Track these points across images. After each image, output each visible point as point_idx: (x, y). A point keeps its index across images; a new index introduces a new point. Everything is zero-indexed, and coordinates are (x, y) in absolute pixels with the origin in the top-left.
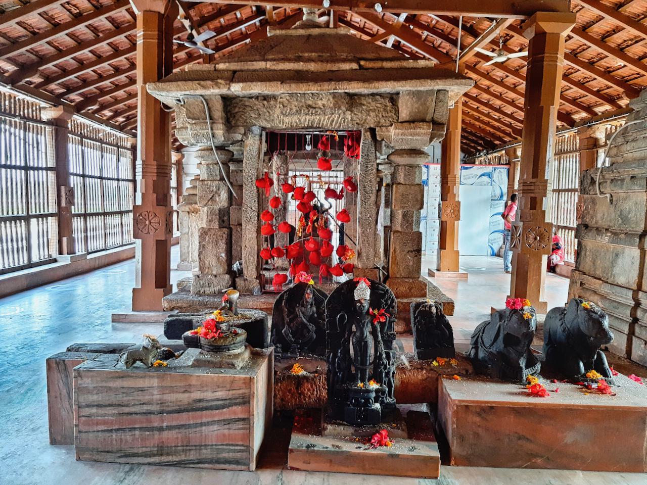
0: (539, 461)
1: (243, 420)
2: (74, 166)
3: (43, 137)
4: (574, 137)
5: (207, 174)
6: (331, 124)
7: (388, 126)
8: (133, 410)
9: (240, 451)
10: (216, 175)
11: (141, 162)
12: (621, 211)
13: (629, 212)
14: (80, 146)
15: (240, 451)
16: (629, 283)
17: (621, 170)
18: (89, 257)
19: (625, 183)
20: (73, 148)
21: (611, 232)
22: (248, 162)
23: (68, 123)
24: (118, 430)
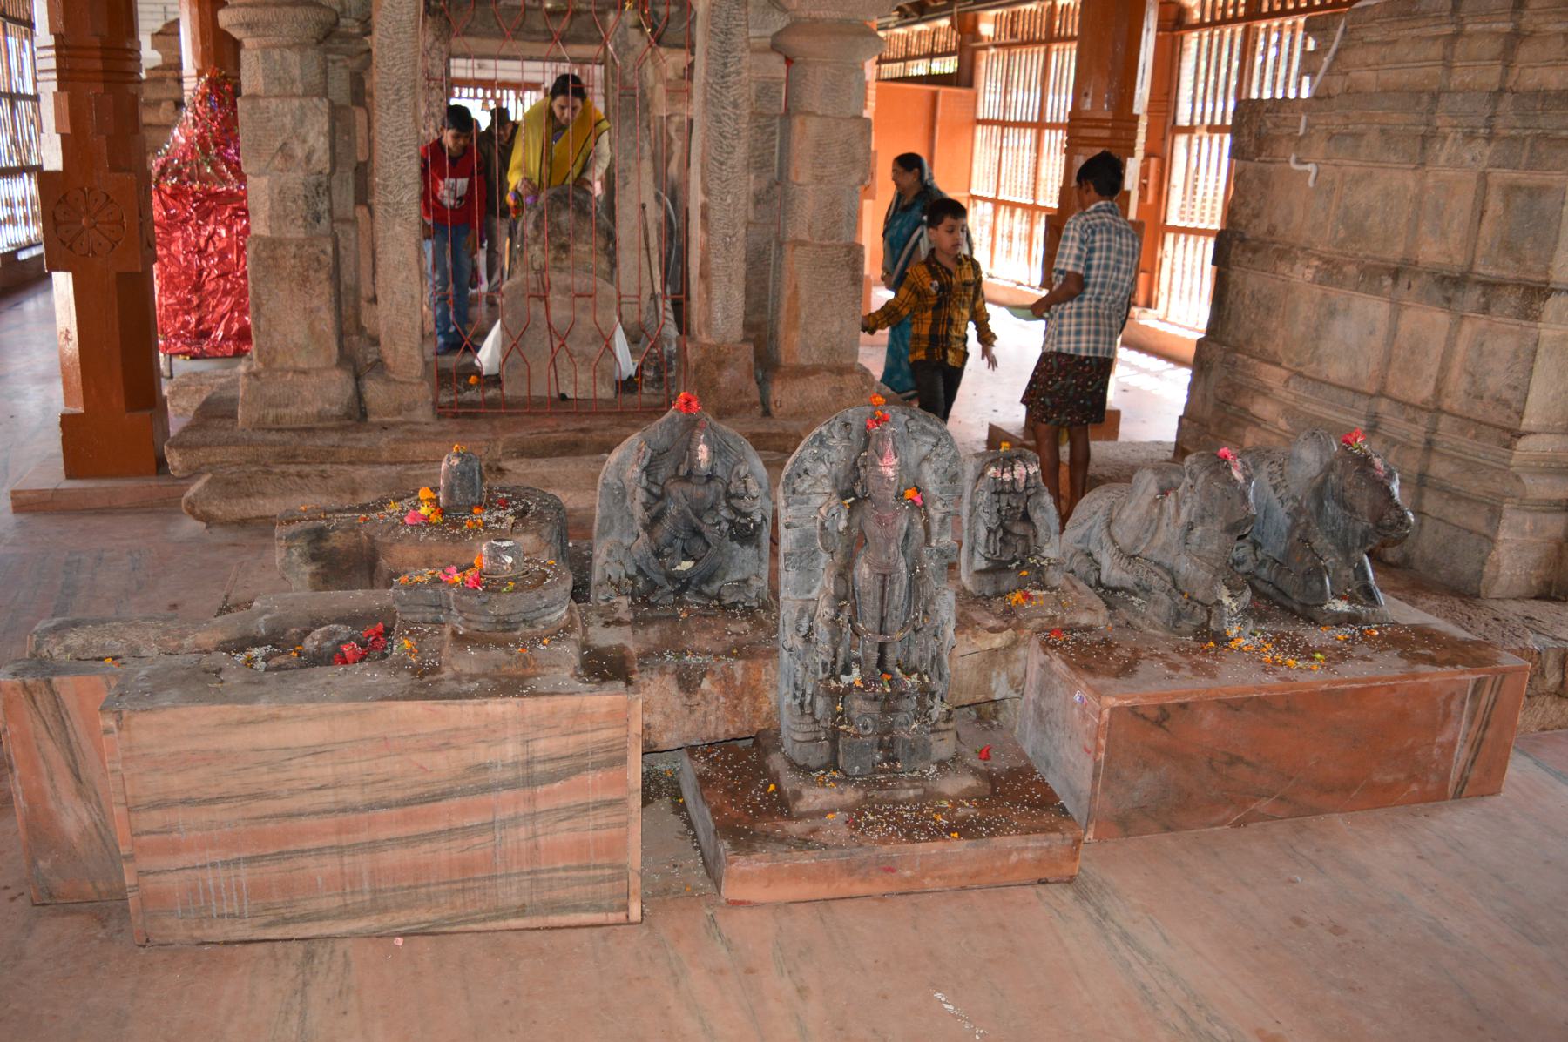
0: (1264, 805)
1: (610, 803)
5: (266, 76)
8: (292, 804)
9: (597, 881)
10: (293, 82)
11: (51, 41)
12: (1347, 208)
13: (1367, 215)
15: (597, 881)
16: (1356, 376)
19: (1364, 143)
22: (387, 41)
24: (251, 860)
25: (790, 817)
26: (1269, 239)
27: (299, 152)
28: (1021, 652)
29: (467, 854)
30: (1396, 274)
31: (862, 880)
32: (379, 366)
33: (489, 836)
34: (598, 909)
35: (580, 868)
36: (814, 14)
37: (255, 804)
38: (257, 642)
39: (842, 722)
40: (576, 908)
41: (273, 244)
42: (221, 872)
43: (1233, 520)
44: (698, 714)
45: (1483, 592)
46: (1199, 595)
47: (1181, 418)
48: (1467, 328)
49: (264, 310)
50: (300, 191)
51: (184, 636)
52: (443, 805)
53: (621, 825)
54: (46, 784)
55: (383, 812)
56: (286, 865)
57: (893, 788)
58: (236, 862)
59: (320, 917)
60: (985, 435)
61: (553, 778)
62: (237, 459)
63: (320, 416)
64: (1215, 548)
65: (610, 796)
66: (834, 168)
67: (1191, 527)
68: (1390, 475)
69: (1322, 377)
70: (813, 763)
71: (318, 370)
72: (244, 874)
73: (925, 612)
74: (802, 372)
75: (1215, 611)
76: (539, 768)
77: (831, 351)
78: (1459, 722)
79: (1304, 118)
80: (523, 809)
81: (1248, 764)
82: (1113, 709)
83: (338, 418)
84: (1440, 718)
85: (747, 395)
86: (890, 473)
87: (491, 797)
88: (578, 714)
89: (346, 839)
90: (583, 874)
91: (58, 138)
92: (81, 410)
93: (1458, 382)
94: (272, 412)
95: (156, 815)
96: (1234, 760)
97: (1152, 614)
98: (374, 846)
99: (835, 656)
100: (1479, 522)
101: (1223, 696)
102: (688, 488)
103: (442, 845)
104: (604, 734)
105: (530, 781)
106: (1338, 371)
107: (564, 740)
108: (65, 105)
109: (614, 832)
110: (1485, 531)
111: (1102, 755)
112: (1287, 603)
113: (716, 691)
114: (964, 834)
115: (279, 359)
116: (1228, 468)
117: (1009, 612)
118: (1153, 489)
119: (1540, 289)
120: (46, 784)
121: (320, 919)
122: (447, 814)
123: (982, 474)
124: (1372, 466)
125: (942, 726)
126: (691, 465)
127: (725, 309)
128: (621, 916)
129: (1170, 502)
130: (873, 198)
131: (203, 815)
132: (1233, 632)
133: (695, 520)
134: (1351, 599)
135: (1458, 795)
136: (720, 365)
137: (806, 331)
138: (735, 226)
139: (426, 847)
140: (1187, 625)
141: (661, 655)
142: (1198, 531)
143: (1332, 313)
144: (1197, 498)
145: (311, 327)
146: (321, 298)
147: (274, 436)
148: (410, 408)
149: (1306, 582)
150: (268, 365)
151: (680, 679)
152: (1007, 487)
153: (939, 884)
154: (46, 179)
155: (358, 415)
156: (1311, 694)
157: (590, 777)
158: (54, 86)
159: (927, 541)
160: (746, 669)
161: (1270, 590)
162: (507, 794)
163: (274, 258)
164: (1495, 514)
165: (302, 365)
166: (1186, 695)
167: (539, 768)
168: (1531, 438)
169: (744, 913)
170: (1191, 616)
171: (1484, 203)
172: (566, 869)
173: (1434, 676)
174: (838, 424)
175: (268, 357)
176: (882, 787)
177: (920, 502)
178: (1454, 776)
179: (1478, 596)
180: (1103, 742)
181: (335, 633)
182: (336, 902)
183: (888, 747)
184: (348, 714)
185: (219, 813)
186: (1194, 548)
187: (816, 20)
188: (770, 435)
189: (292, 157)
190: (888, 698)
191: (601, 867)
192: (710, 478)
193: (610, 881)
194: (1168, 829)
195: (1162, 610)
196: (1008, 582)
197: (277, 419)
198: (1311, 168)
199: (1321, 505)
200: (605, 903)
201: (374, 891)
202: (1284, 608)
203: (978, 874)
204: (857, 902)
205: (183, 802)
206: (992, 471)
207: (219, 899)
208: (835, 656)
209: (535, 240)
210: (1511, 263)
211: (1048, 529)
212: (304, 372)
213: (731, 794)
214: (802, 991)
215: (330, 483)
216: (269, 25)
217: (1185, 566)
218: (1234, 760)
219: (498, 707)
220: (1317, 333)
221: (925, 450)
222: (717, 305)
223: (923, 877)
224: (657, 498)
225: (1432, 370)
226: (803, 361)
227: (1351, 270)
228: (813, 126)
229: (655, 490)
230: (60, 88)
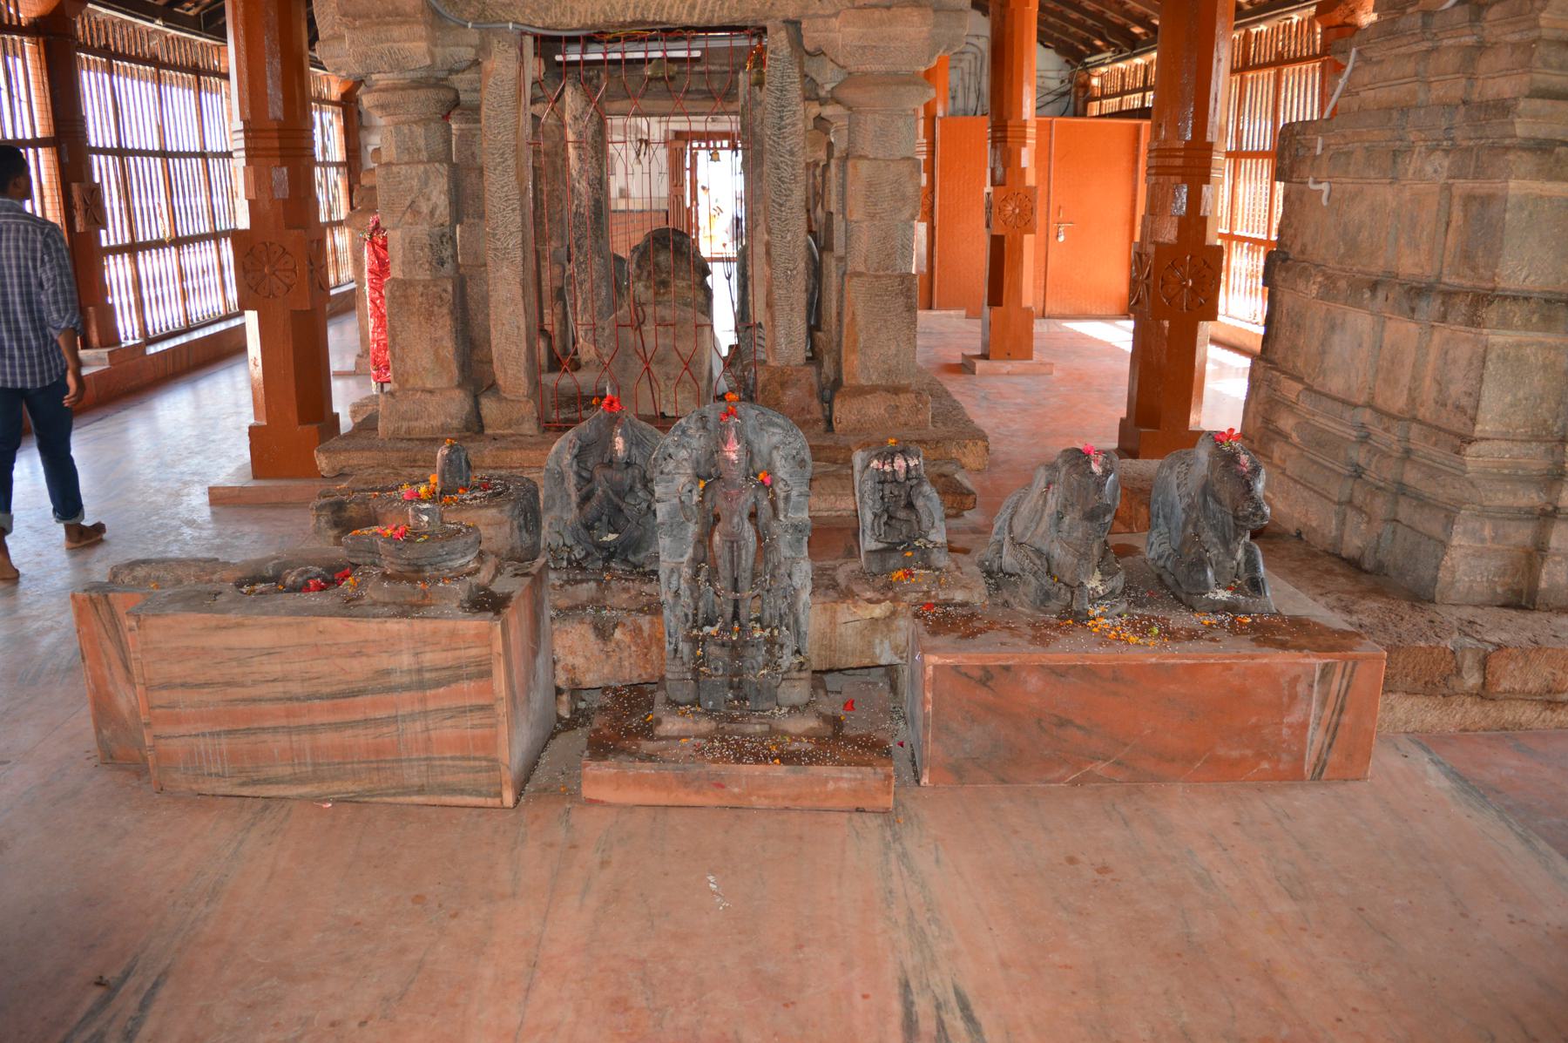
0: (1100, 768)
1: (482, 708)
2: (99, 132)
3: (19, 61)
4: (1311, 22)
5: (398, 147)
6: (690, 14)
7: (829, 16)
9: (478, 771)
10: (419, 150)
11: (240, 126)
13: (1359, 231)
14: (106, 76)
15: (478, 771)
17: (1348, 132)
18: (152, 350)
20: (92, 84)
21: (1324, 274)
23: (75, 23)
24: (229, 732)
25: (651, 739)
26: (1301, 257)
27: (425, 209)
29: (379, 740)
30: (1374, 286)
31: (697, 792)
32: (493, 387)
33: (393, 728)
34: (479, 793)
35: (463, 758)
36: (862, 68)
37: (230, 690)
38: (264, 580)
39: (702, 665)
40: (462, 792)
41: (405, 284)
42: (208, 740)
43: (1088, 508)
44: (614, 659)
45: (1438, 598)
48: (1437, 338)
49: (399, 339)
50: (426, 240)
51: (213, 573)
52: (359, 699)
53: (491, 726)
54: (106, 672)
55: (317, 702)
56: (252, 738)
58: (219, 734)
59: (277, 781)
61: (438, 684)
62: (370, 462)
65: (481, 702)
66: (885, 205)
68: (1256, 471)
69: (1326, 390)
70: (681, 699)
71: (441, 389)
72: (224, 743)
73: (773, 576)
74: (861, 391)
76: (427, 675)
77: (889, 372)
78: (1309, 705)
79: (1320, 140)
80: (417, 708)
81: (1079, 727)
82: (936, 667)
83: (459, 430)
84: (1285, 699)
86: (734, 457)
87: (394, 696)
88: (453, 634)
89: (294, 722)
90: (465, 763)
91: (246, 203)
92: (264, 423)
93: (1429, 390)
94: (405, 425)
95: (165, 693)
96: (1063, 723)
98: (312, 729)
99: (696, 609)
100: (1436, 528)
102: (608, 473)
103: (361, 731)
104: (473, 652)
105: (422, 686)
106: (1336, 384)
107: (444, 655)
108: (251, 178)
109: (487, 731)
110: (1442, 537)
113: (627, 639)
114: (783, 761)
115: (411, 380)
119: (1486, 295)
120: (106, 672)
121: (277, 783)
122: (363, 707)
124: (1237, 462)
125: (795, 674)
127: (788, 335)
128: (497, 801)
130: (1032, 231)
131: (195, 696)
133: (616, 499)
134: (1237, 590)
135: (1318, 775)
136: (783, 385)
137: (864, 354)
138: (795, 260)
139: (349, 732)
141: (584, 609)
142: (1067, 520)
143: (1333, 328)
145: (436, 353)
146: (444, 329)
147: (403, 445)
148: (519, 423)
150: (402, 386)
151: (596, 628)
152: (889, 477)
153: (765, 803)
154: (236, 236)
155: (476, 428)
156: (1137, 666)
157: (465, 685)
158: (243, 162)
159: (776, 515)
160: (652, 623)
162: (406, 695)
163: (405, 297)
164: (1450, 520)
165: (429, 386)
167: (427, 675)
168: (1483, 445)
169: (596, 810)
170: (1057, 596)
171: (1449, 214)
172: (452, 758)
173: (1278, 659)
175: (402, 380)
176: (733, 720)
177: (768, 483)
178: (1310, 758)
179: (1432, 601)
181: (307, 572)
182: (288, 770)
183: (737, 686)
184: (289, 625)
185: (205, 695)
186: (1064, 535)
187: (865, 74)
189: (420, 213)
191: (479, 759)
192: (628, 464)
193: (488, 771)
194: (1003, 781)
195: (1031, 589)
196: (894, 560)
197: (409, 431)
198: (1325, 187)
199: (1205, 500)
200: (484, 789)
201: (315, 764)
203: (798, 797)
204: (686, 811)
205: (182, 685)
206: (875, 464)
207: (208, 761)
208: (696, 609)
209: (639, 278)
210: (1468, 272)
211: (931, 514)
212: (431, 392)
213: (614, 723)
214: (604, 864)
216: (397, 105)
217: (1057, 552)
218: (1063, 723)
219: (396, 626)
220: (1325, 344)
221: (775, 439)
222: (781, 332)
223: (750, 795)
224: (585, 481)
225: (1405, 380)
226: (863, 382)
227: (1342, 284)
228: (864, 166)
229: (584, 474)
230: (248, 163)
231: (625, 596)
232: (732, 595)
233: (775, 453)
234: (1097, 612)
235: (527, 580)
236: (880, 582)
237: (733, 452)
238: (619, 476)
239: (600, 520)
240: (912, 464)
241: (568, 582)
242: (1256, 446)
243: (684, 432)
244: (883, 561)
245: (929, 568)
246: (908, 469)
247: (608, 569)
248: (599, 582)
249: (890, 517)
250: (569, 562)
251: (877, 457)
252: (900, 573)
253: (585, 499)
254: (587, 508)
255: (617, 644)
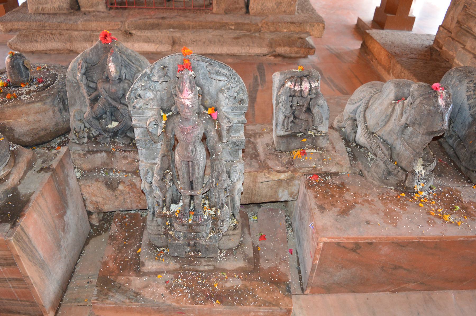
0: (411, 285)
28: (296, 182)
39: (170, 230)
44: (121, 198)
46: (404, 164)
47: (440, 26)
57: (195, 265)
60: (355, 22)
63: (60, 8)
64: (418, 140)
67: (406, 126)
70: (159, 245)
75: (410, 176)
81: (405, 269)
82: (325, 243)
85: (238, 4)
86: (188, 103)
97: (377, 166)
101: (396, 240)
102: (107, 86)
111: (317, 262)
112: (458, 164)
113: (127, 190)
116: (436, 97)
117: (291, 163)
118: (392, 96)
123: (283, 85)
125: (231, 232)
126: (108, 73)
129: (399, 106)
132: (418, 188)
140: (393, 180)
141: (99, 172)
142: (410, 129)
144: (413, 111)
148: (97, 4)
149: (471, 158)
151: (106, 184)
161: (451, 152)
166: (372, 239)
174: (157, 67)
177: (215, 117)
180: (318, 257)
186: (406, 137)
188: (244, 24)
190: (190, 225)
196: (294, 144)
197: (43, 9)
202: (456, 166)
206: (289, 84)
211: (321, 117)
215: (63, 37)
217: (399, 146)
224: (92, 89)
229: (92, 85)
231: (125, 162)
232: (189, 193)
233: (220, 95)
234: (419, 187)
235: (47, 175)
236: (285, 158)
237: (188, 99)
238: (114, 88)
239: (106, 113)
240: (313, 86)
241: (88, 152)
242: (453, 35)
243: (149, 78)
244: (288, 144)
245: (315, 148)
246: (311, 89)
247: (114, 143)
248: (108, 152)
249: (295, 118)
250: (89, 138)
251: (290, 79)
252: (298, 153)
253: (95, 100)
254: (96, 107)
255: (121, 191)
